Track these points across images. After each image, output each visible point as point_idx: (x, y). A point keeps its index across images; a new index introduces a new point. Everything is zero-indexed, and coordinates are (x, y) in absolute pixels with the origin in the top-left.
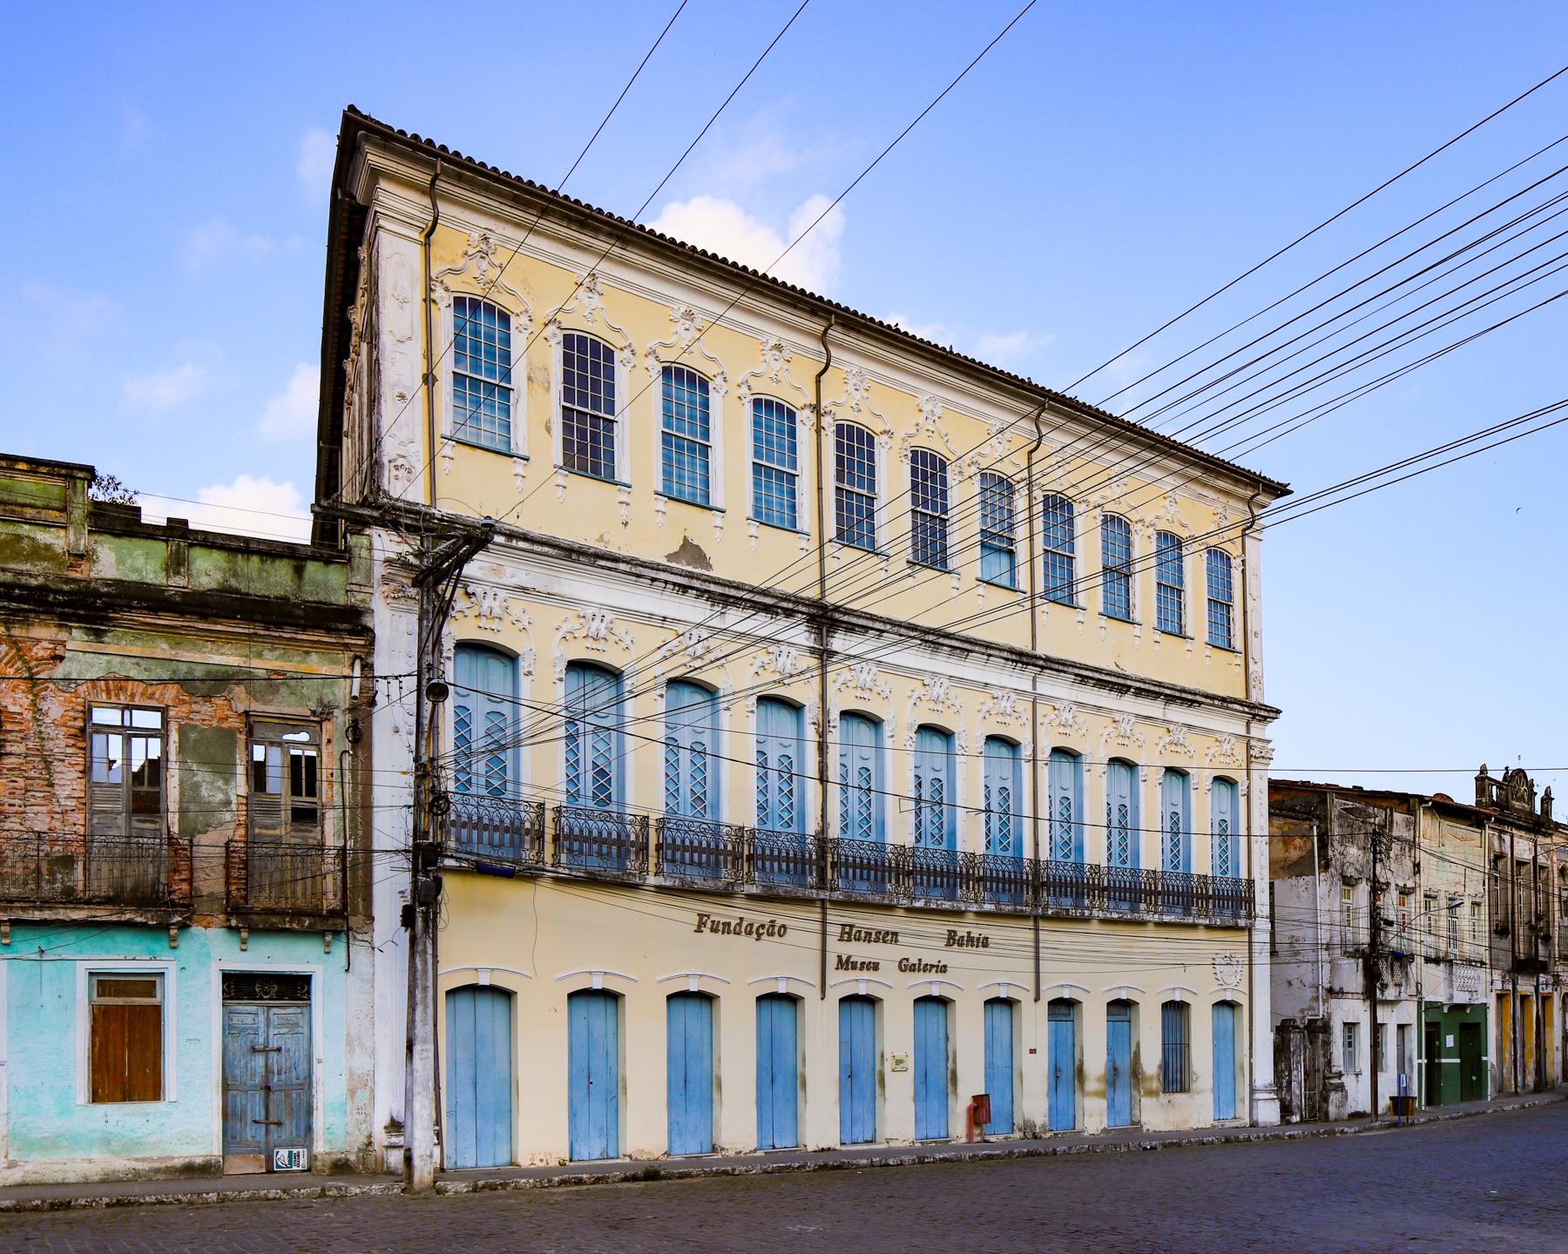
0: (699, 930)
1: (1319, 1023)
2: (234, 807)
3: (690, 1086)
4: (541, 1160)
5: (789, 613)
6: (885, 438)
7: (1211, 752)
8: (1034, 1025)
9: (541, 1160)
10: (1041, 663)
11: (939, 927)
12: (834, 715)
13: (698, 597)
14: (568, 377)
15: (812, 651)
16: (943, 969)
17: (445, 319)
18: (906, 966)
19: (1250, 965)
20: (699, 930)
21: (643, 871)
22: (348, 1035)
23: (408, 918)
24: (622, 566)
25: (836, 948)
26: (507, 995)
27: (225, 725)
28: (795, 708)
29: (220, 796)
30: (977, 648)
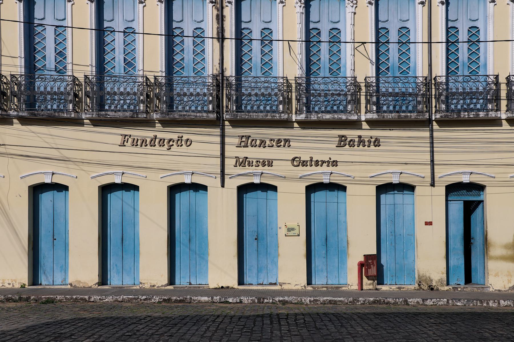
3: (126, 243)
4: (9, 284)
9: (9, 284)
16: (335, 163)
21: (288, 110)
25: (231, 151)
26: (136, 188)
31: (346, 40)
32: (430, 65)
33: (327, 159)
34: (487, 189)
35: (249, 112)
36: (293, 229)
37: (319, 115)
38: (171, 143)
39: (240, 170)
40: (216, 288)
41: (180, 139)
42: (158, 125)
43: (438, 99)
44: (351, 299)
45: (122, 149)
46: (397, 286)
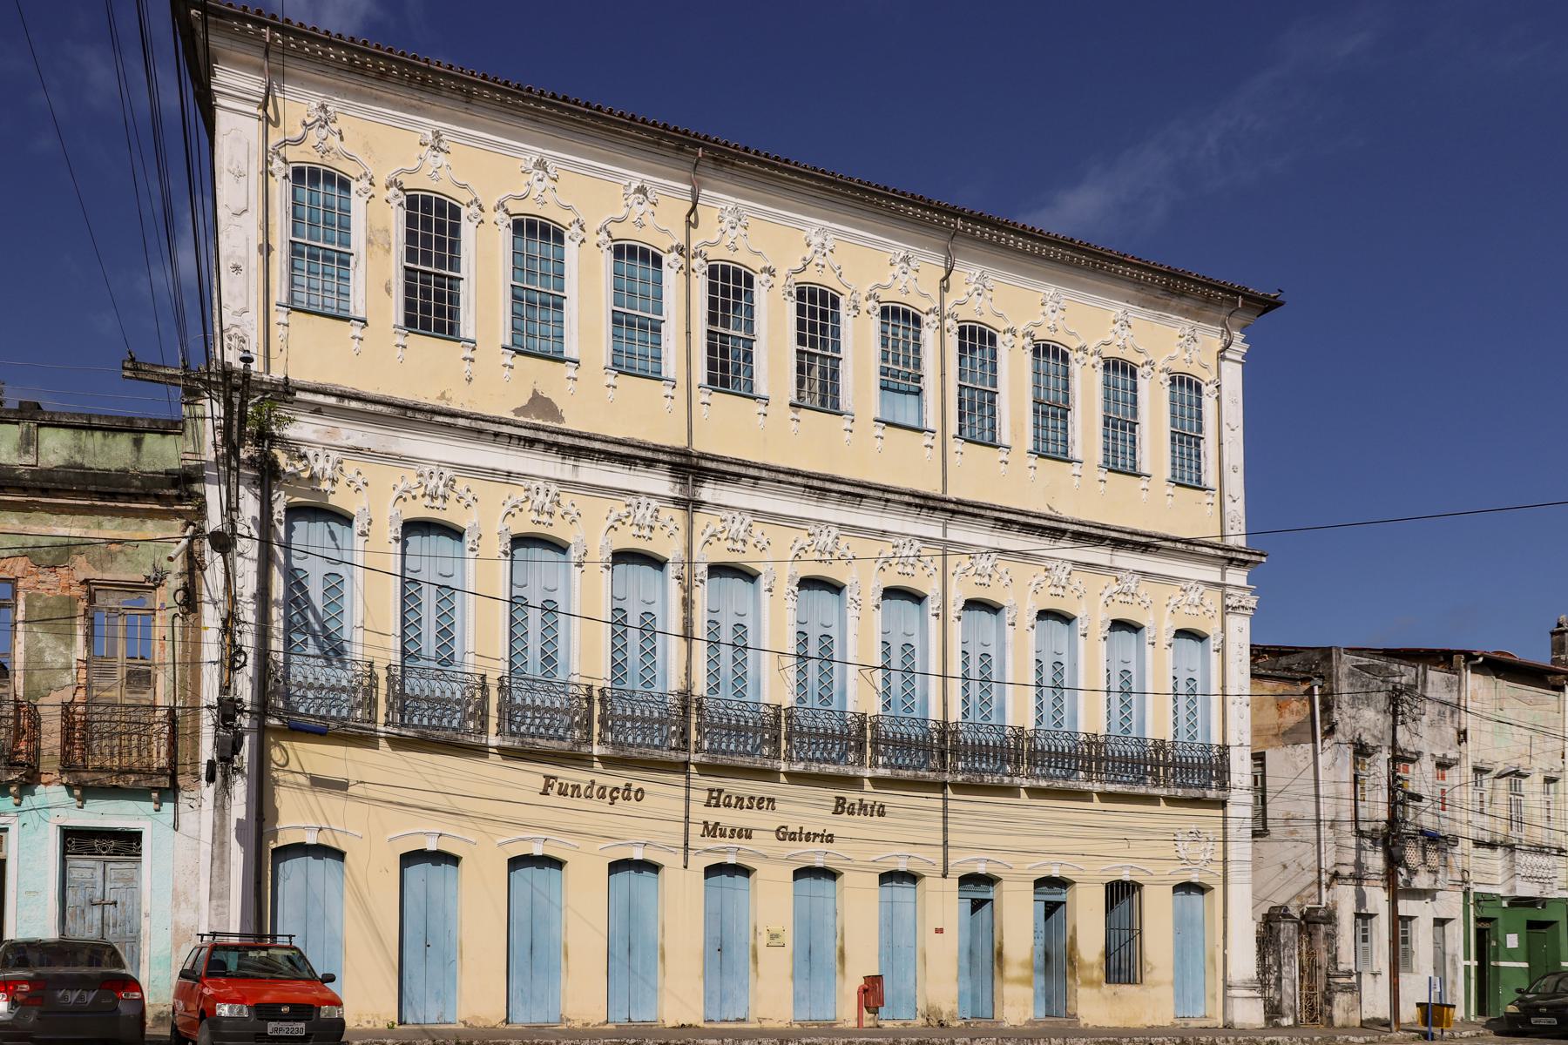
4: (369, 1022)
5: (650, 463)
9: (369, 1022)
10: (951, 506)
12: (702, 569)
14: (411, 237)
15: (676, 501)
16: (830, 838)
17: (281, 189)
18: (783, 834)
21: (483, 729)
24: (461, 422)
30: (871, 493)
31: (759, 644)
32: (945, 705)
33: (821, 832)
34: (1005, 885)
35: (732, 753)
36: (777, 936)
37: (822, 766)
38: (615, 794)
39: (709, 843)
40: (674, 1027)
41: (628, 787)
42: (598, 766)
43: (789, 740)
44: (891, 1040)
45: (544, 800)
46: (902, 1022)
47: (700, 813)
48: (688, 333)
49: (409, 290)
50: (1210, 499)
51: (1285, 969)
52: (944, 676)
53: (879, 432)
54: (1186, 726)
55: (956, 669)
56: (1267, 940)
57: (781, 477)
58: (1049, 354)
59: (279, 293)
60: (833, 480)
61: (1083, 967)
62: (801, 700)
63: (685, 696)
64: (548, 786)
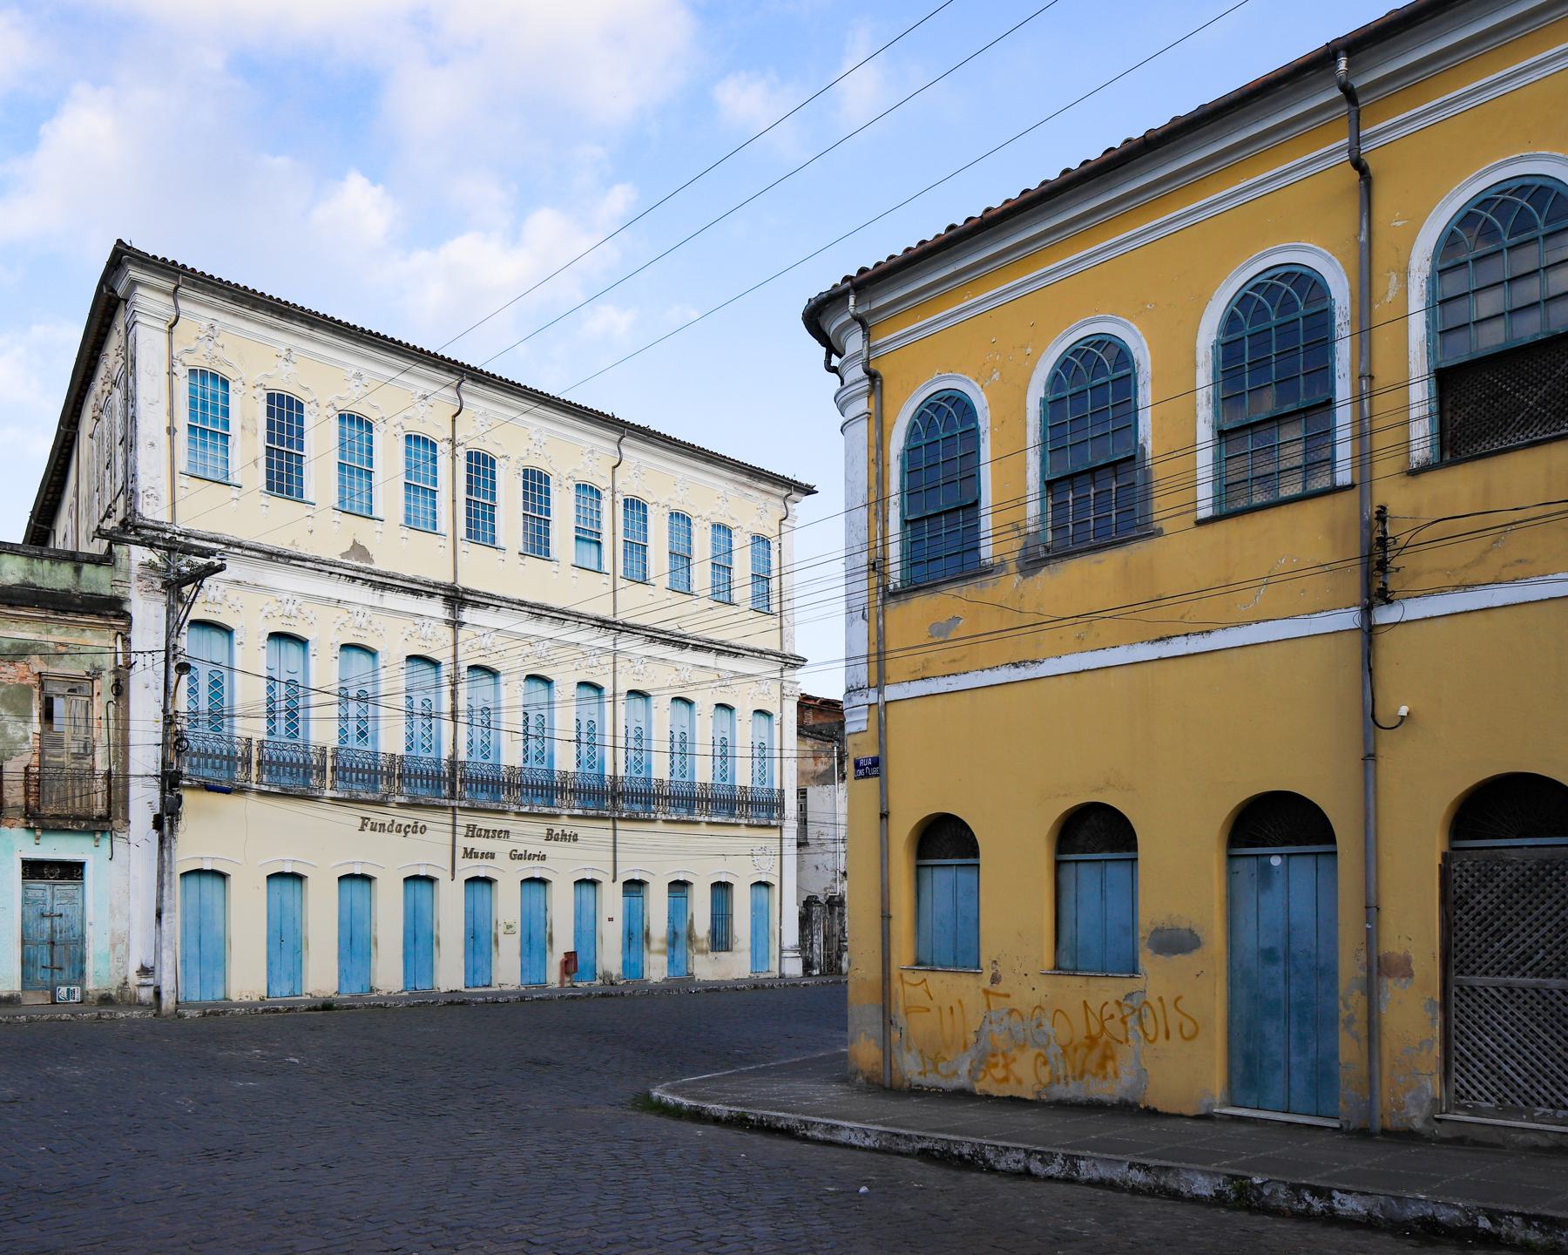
0: (362, 829)
1: (837, 899)
2: (31, 741)
5: (431, 595)
6: (503, 460)
7: (752, 691)
8: (612, 900)
10: (620, 627)
11: (539, 828)
12: (463, 670)
13: (363, 584)
14: (270, 425)
15: (447, 622)
16: (544, 858)
17: (182, 385)
18: (515, 856)
19: (781, 855)
20: (362, 829)
21: (322, 787)
22: (111, 905)
23: (158, 823)
24: (309, 564)
26: (223, 876)
27: (25, 682)
28: (435, 664)
29: (21, 733)
30: (571, 618)
36: (511, 926)
47: (463, 842)
48: (454, 501)
49: (269, 463)
50: (605, 580)
51: (816, 937)
52: (614, 747)
53: (575, 574)
54: (534, 753)
55: (621, 742)
56: (805, 921)
57: (515, 606)
58: (355, 424)
59: (182, 465)
60: (547, 609)
61: (696, 941)
62: (342, 741)
63: (453, 762)
64: (364, 824)
